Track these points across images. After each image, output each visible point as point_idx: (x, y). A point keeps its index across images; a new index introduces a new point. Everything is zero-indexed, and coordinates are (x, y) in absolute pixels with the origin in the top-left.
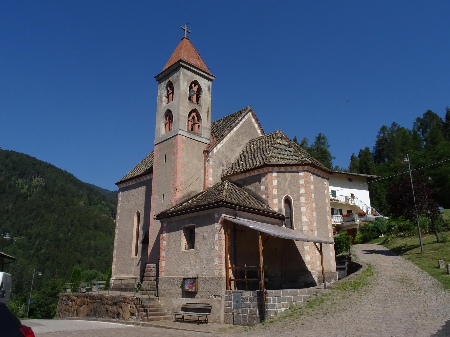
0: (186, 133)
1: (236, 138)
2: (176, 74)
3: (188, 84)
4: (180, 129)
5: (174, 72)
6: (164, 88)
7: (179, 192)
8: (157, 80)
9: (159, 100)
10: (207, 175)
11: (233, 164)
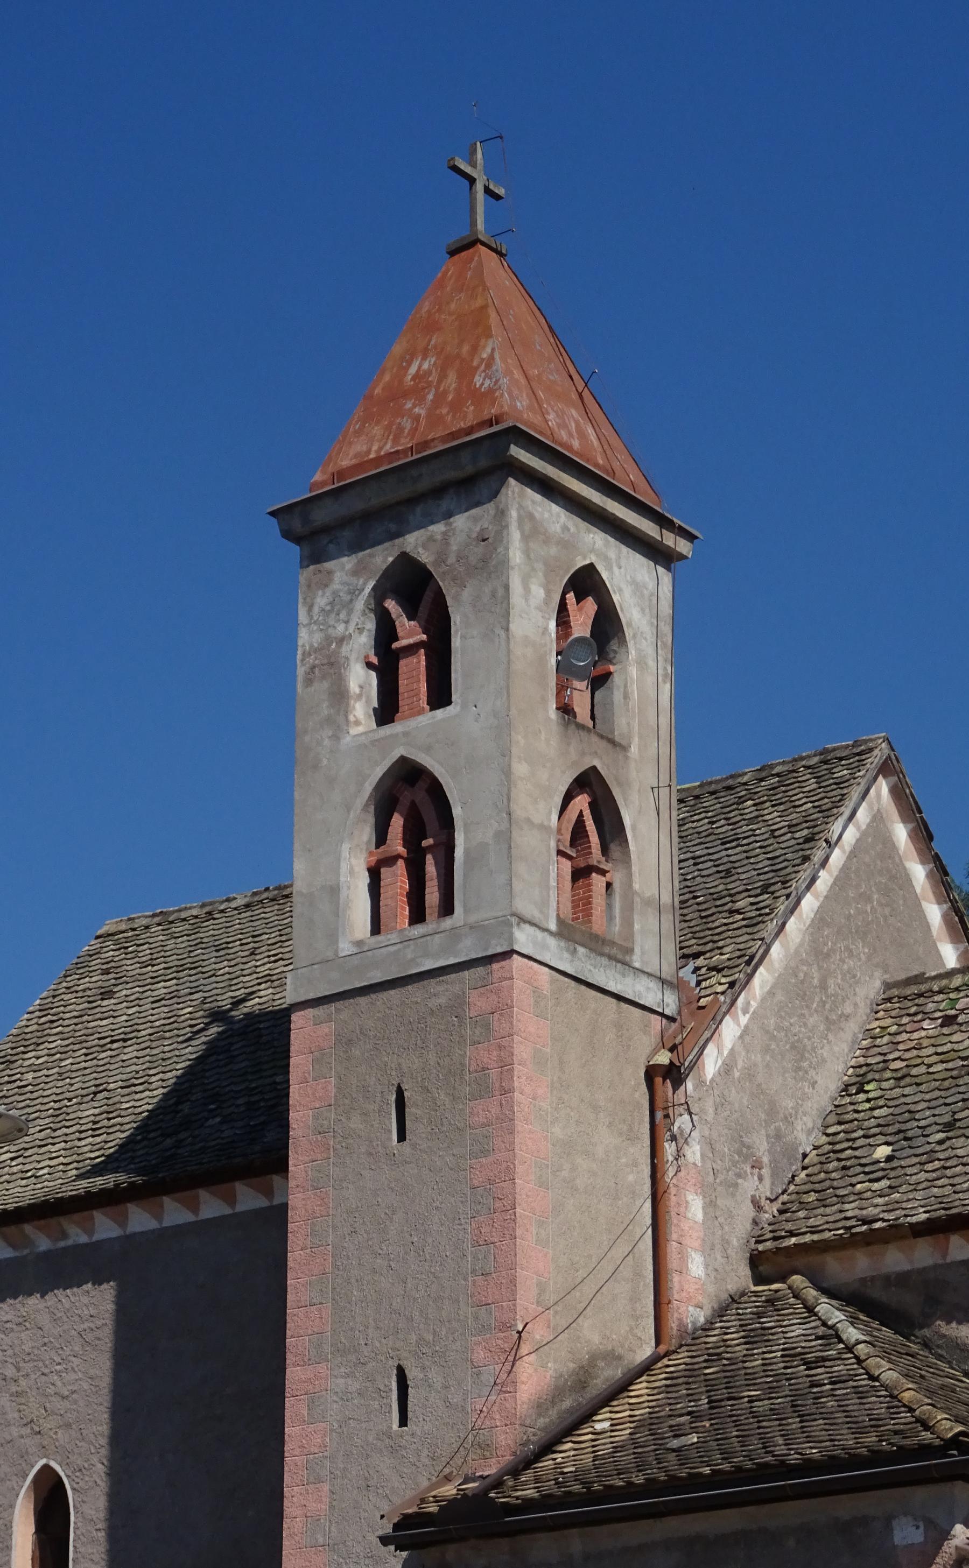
0: (552, 942)
1: (814, 969)
2: (461, 521)
3: (548, 592)
4: (522, 920)
5: (446, 503)
6: (360, 604)
7: (533, 1356)
8: (287, 534)
9: (309, 682)
10: (674, 1236)
11: (805, 1156)
